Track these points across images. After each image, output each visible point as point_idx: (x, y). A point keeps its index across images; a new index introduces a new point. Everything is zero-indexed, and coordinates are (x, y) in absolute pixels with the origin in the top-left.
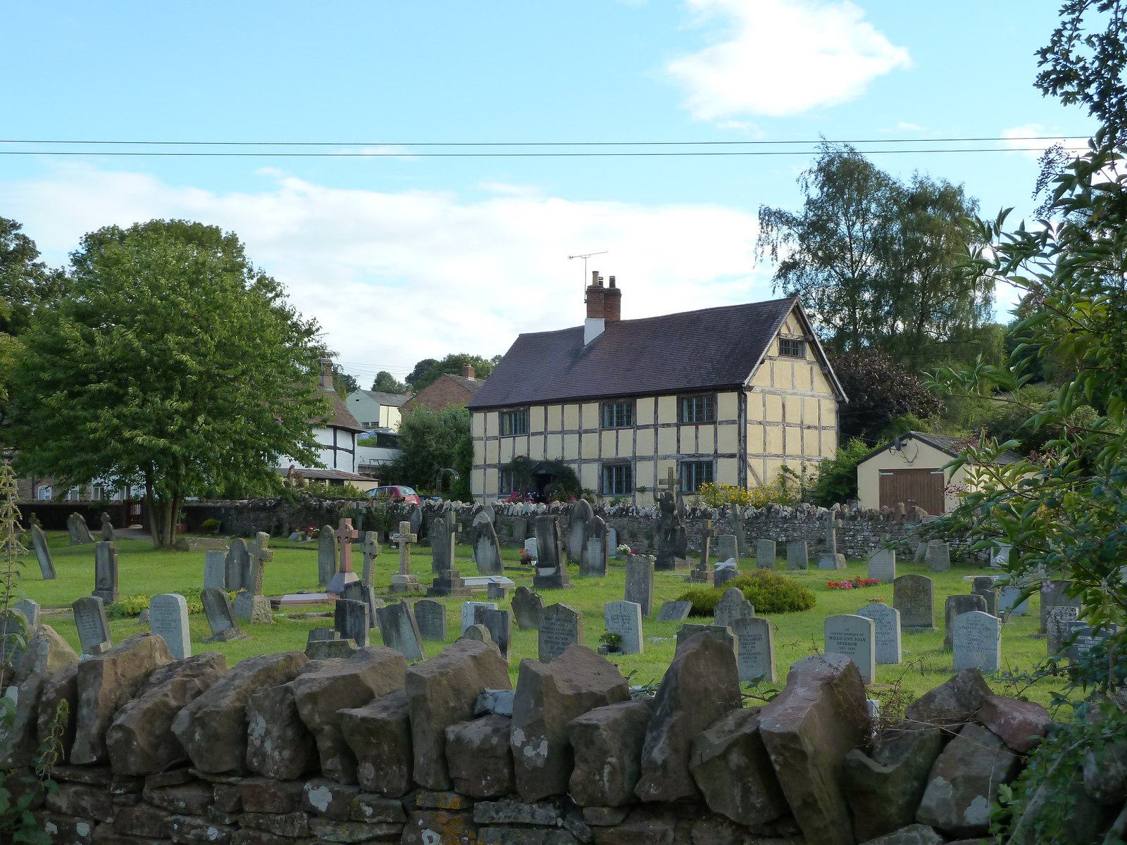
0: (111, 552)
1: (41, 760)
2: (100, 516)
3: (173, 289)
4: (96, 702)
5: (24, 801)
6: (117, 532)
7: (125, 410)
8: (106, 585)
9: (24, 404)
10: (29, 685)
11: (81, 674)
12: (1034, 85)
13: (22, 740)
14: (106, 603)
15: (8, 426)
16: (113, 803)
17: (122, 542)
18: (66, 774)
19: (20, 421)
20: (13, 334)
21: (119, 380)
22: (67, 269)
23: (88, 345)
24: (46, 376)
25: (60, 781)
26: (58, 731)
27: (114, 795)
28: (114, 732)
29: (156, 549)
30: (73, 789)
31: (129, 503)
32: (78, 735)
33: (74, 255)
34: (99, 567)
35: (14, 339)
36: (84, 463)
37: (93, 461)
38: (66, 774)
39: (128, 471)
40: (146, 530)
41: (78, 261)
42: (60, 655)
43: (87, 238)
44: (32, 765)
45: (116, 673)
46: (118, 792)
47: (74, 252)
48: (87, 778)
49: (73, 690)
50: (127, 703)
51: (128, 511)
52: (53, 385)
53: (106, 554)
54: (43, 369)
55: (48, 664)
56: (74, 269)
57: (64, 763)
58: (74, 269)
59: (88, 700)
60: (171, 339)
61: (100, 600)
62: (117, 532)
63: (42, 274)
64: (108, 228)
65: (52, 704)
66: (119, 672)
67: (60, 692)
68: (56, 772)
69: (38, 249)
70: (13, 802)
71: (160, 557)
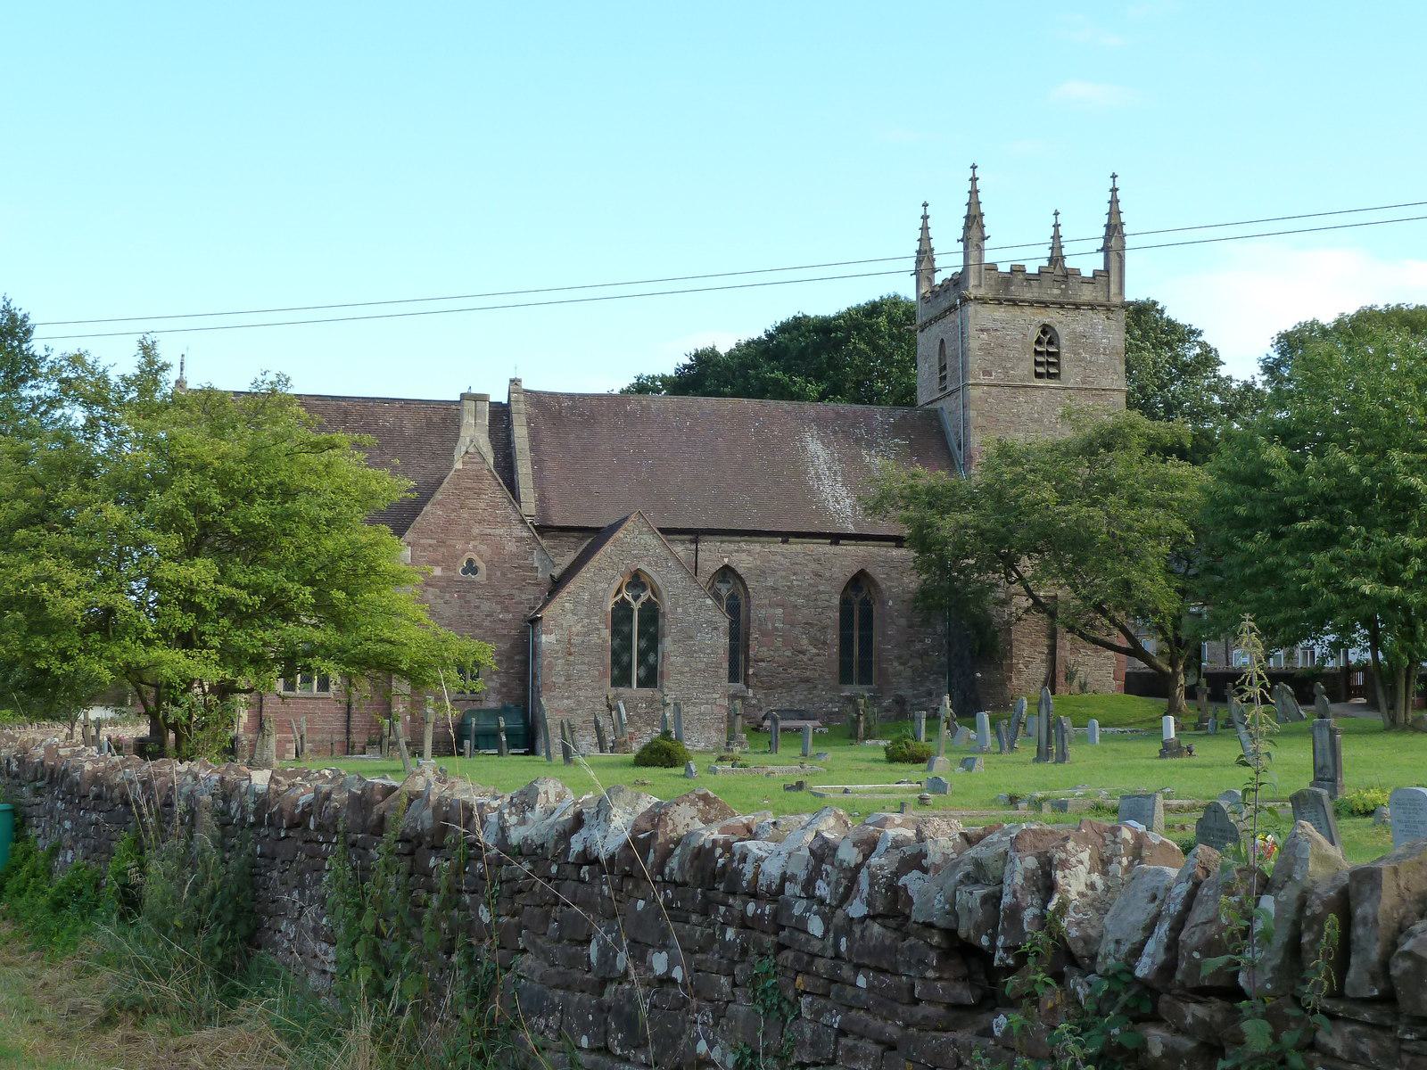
0: (1333, 732)
1: (1308, 989)
2: (1312, 687)
3: (1397, 393)
4: (1376, 921)
5: (1288, 1038)
6: (1335, 708)
7: (1345, 553)
8: (1327, 773)
9: (1212, 549)
10: (1290, 894)
11: (1354, 884)
12: (515, 382)
13: (1283, 962)
14: (1331, 798)
15: (1196, 576)
16: (1401, 1051)
17: (1342, 720)
18: (1340, 1008)
19: (1210, 570)
20: (1194, 463)
21: (1332, 513)
22: (1257, 378)
23: (1294, 472)
24: (1241, 510)
25: (1332, 1017)
26: (1327, 954)
27: (1402, 1041)
28: (1400, 961)
29: (1387, 730)
30: (1348, 1029)
31: (1348, 670)
32: (1353, 960)
33: (1263, 360)
34: (1317, 751)
35: (1196, 469)
36: (1287, 622)
37: (1302, 618)
38: (1340, 1008)
39: (1346, 630)
40: (1373, 705)
41: (1270, 368)
42: (1324, 859)
43: (1279, 338)
44: (1297, 994)
45: (1398, 885)
46: (1408, 1037)
47: (1264, 357)
48: (1366, 1016)
49: (1344, 903)
50: (1413, 924)
51: (1348, 682)
52: (1250, 523)
53: (1326, 734)
54: (1236, 502)
55: (1310, 869)
56: (1265, 378)
57: (1337, 994)
58: (1265, 378)
59: (1365, 918)
60: (1396, 455)
61: (1325, 792)
62: (1335, 708)
63: (1228, 388)
64: (1305, 324)
65: (1318, 920)
66: (1402, 884)
67: (1329, 906)
68: (1327, 1005)
69: (1222, 359)
70: (1275, 1037)
71: (1392, 739)
